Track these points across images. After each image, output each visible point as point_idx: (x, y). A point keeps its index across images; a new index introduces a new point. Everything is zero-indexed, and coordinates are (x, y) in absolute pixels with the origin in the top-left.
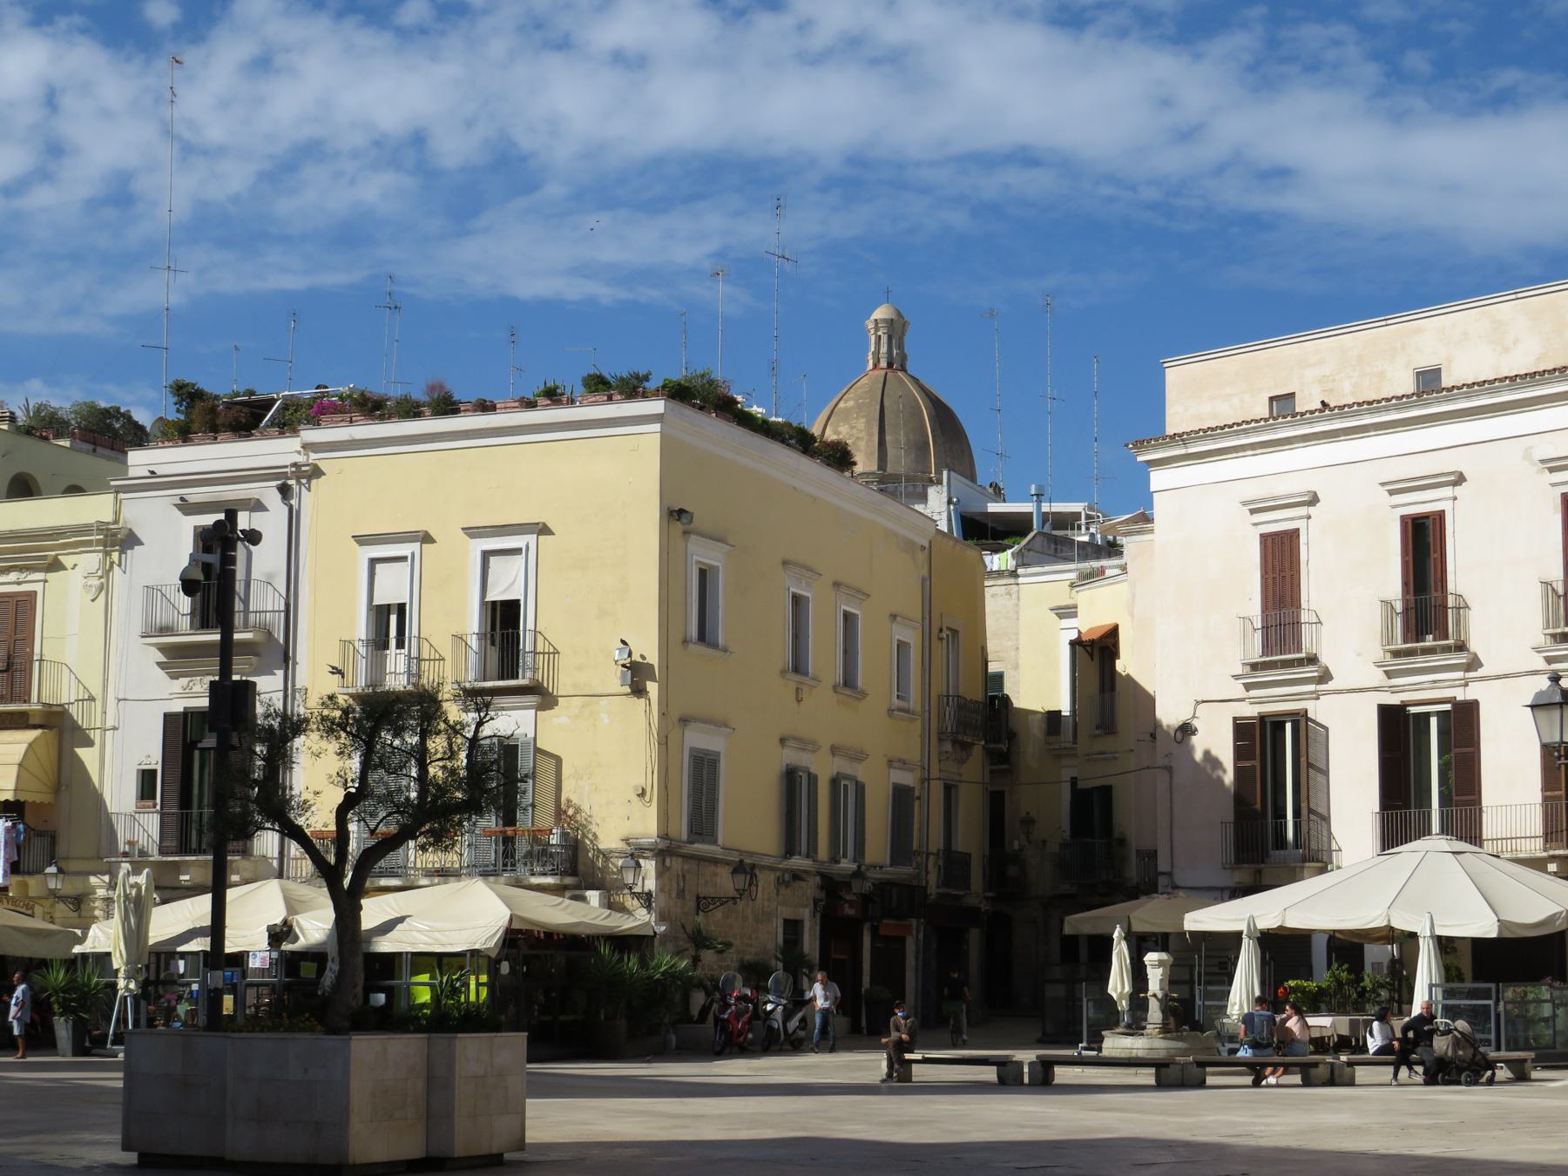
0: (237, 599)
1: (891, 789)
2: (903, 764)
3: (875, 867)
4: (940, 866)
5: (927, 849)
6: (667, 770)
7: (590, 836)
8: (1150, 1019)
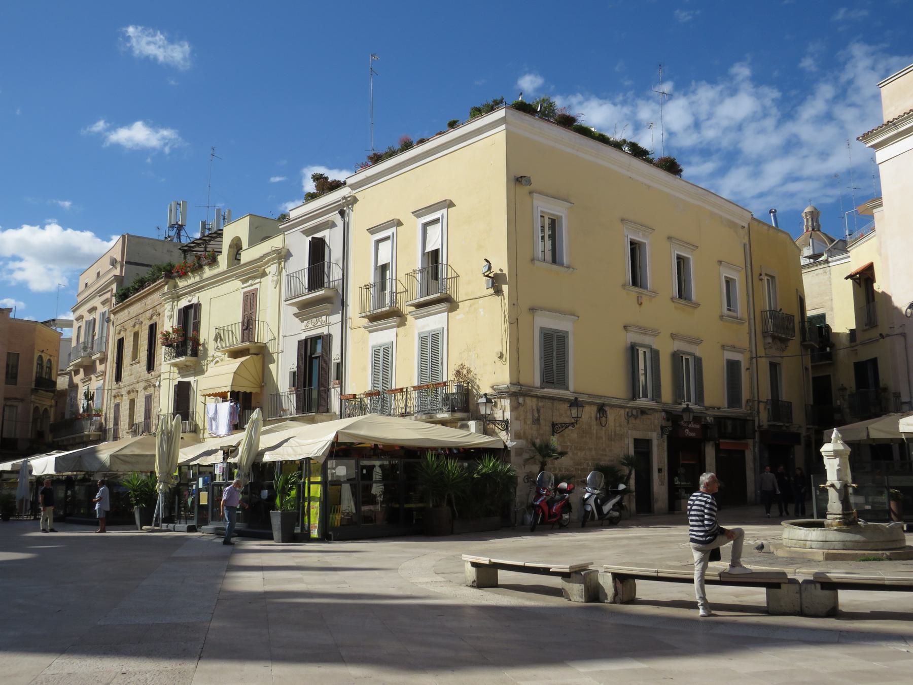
0: (325, 275)
1: (725, 362)
2: (733, 348)
3: (714, 408)
4: (769, 409)
5: (758, 399)
6: (518, 339)
7: (476, 387)
8: (830, 510)
